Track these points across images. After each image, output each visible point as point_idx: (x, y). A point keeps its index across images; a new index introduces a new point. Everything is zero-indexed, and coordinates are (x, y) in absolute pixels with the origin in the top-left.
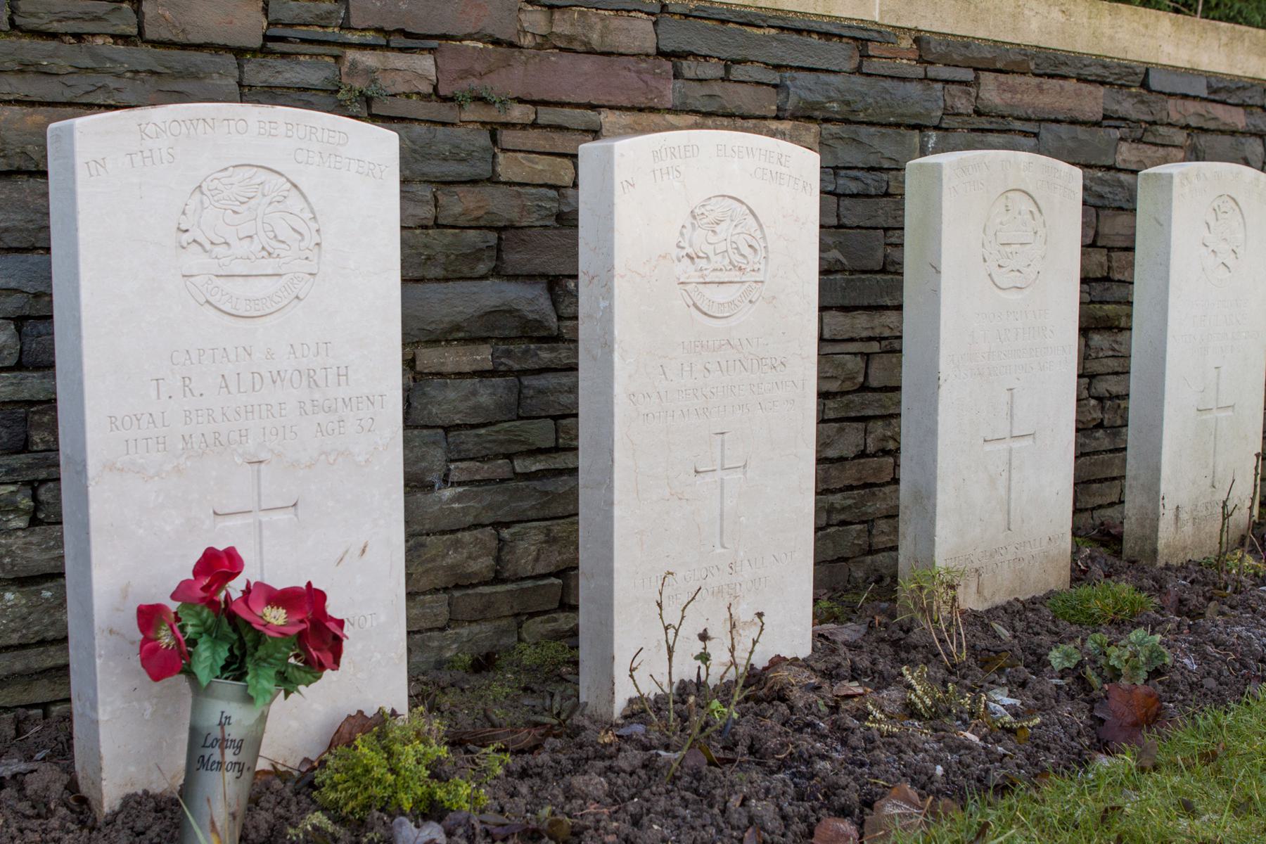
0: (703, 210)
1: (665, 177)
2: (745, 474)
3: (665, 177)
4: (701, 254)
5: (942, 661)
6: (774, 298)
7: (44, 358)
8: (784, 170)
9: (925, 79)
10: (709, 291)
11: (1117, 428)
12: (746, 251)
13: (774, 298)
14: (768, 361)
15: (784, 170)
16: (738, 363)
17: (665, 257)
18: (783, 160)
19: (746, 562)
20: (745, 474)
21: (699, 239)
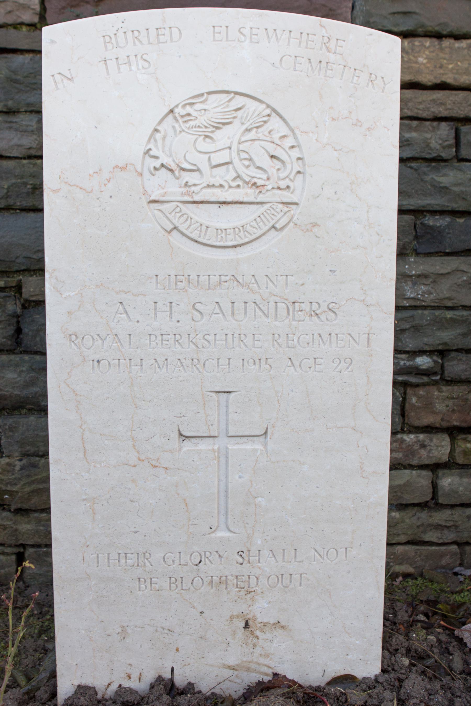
0: (188, 109)
1: (124, 68)
2: (265, 445)
3: (124, 68)
4: (186, 165)
5: (457, 587)
6: (315, 225)
7: (40, 207)
8: (332, 57)
9: (22, 177)
10: (200, 214)
11: (405, 309)
12: (266, 162)
13: (315, 225)
14: (306, 306)
15: (332, 57)
16: (251, 306)
17: (124, 168)
18: (332, 45)
19: (265, 552)
20: (265, 445)
21: (182, 146)
